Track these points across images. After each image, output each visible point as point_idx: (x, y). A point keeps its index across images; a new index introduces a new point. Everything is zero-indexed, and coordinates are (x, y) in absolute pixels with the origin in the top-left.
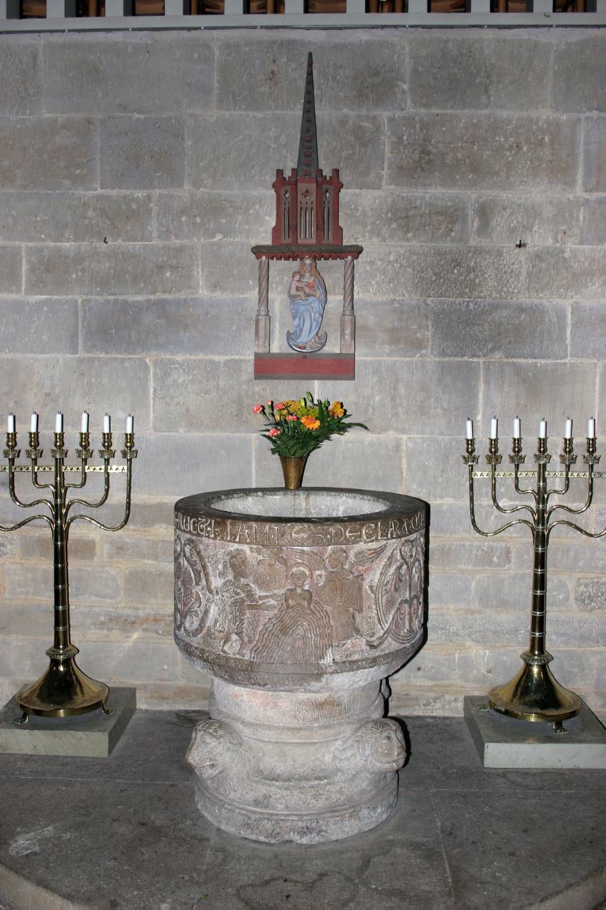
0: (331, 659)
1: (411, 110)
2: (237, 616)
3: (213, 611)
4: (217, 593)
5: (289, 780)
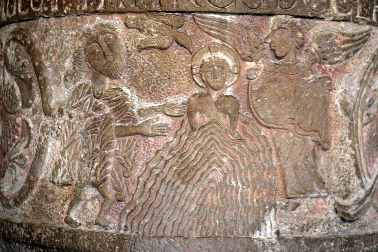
2: (96, 151)
4: (61, 112)
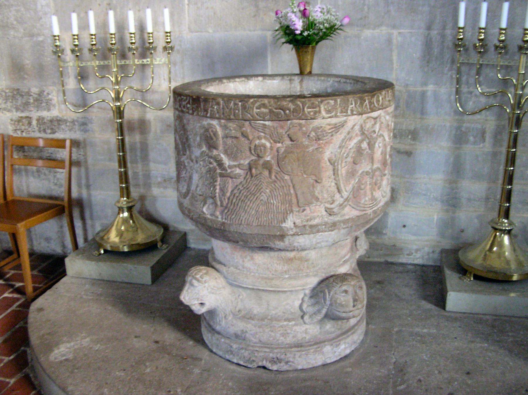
3: (196, 177)
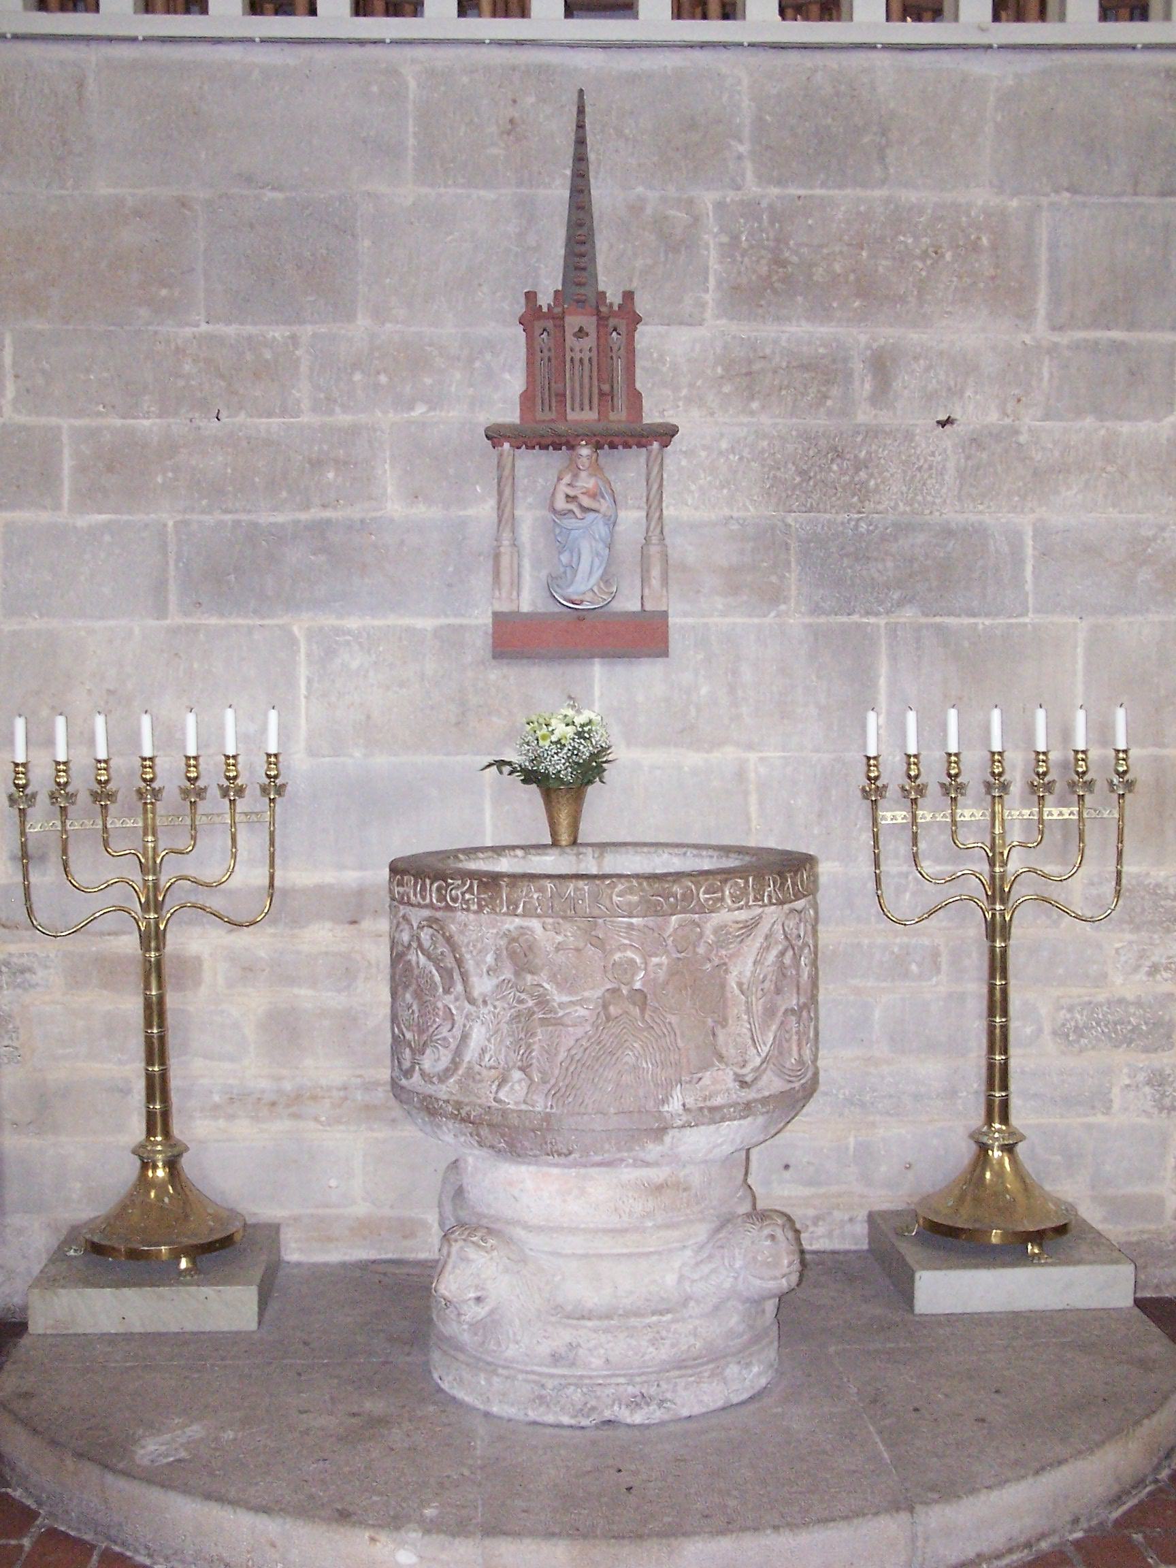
0: (681, 1103)
1: (752, 188)
3: (478, 1035)
4: (485, 1002)
5: (608, 1317)
